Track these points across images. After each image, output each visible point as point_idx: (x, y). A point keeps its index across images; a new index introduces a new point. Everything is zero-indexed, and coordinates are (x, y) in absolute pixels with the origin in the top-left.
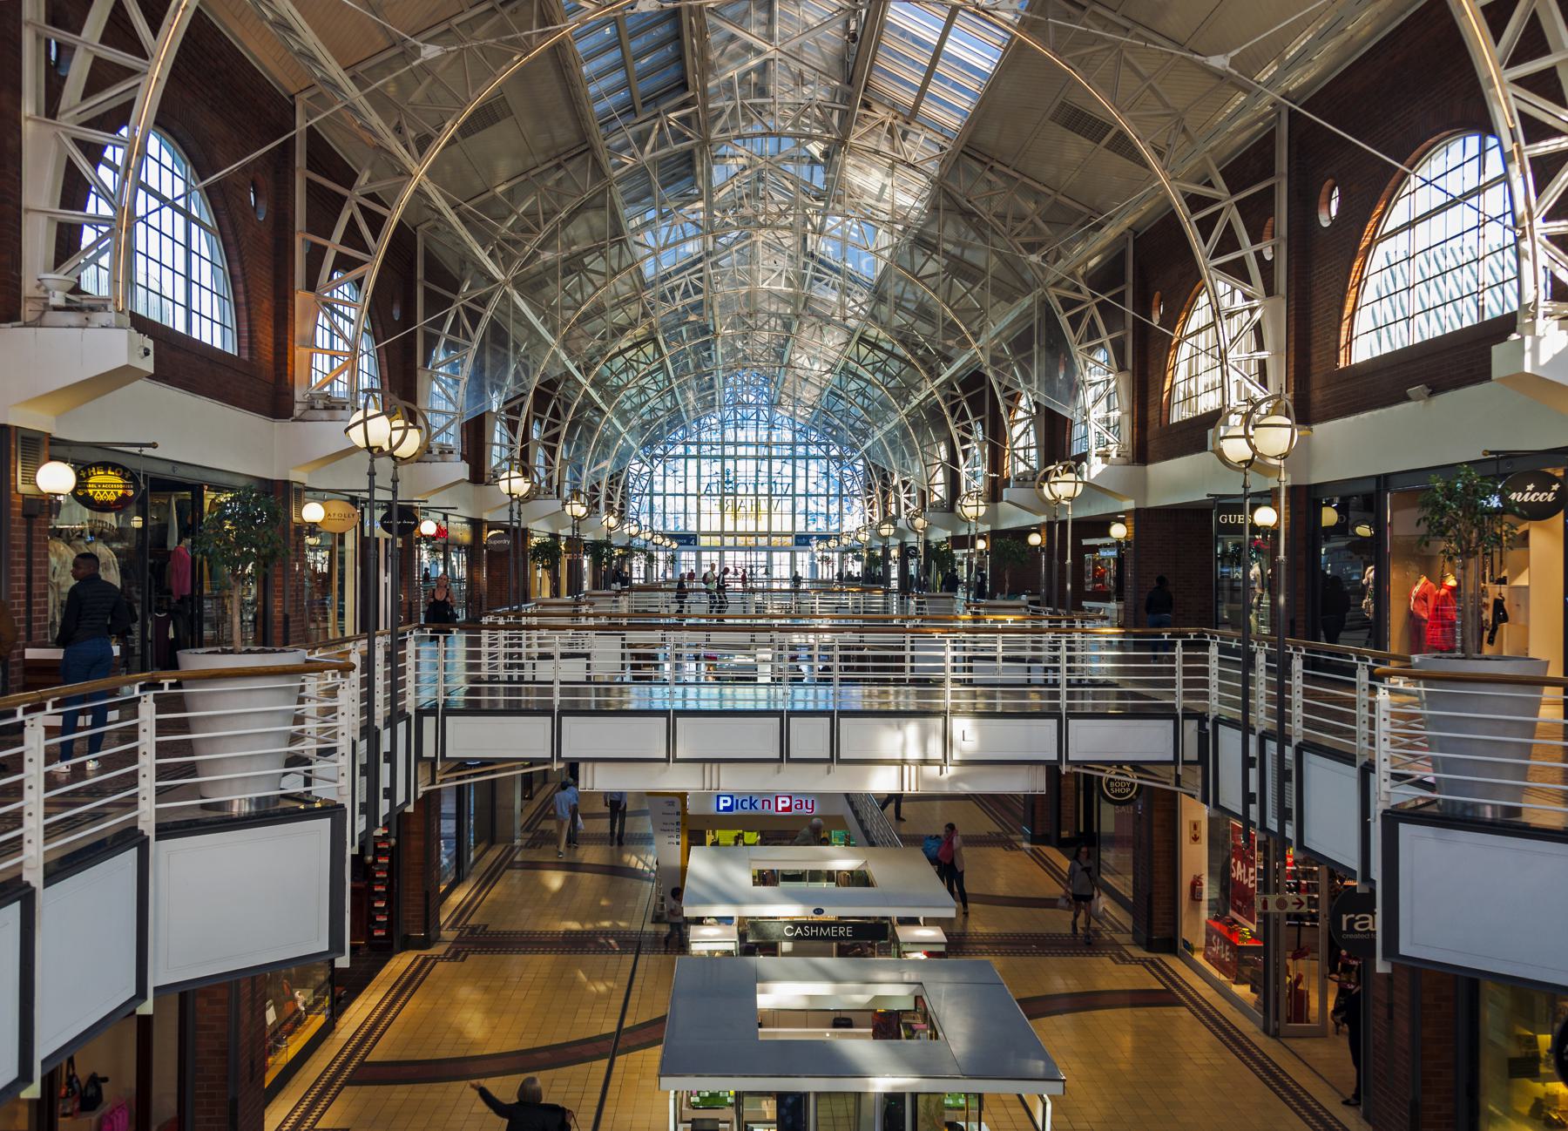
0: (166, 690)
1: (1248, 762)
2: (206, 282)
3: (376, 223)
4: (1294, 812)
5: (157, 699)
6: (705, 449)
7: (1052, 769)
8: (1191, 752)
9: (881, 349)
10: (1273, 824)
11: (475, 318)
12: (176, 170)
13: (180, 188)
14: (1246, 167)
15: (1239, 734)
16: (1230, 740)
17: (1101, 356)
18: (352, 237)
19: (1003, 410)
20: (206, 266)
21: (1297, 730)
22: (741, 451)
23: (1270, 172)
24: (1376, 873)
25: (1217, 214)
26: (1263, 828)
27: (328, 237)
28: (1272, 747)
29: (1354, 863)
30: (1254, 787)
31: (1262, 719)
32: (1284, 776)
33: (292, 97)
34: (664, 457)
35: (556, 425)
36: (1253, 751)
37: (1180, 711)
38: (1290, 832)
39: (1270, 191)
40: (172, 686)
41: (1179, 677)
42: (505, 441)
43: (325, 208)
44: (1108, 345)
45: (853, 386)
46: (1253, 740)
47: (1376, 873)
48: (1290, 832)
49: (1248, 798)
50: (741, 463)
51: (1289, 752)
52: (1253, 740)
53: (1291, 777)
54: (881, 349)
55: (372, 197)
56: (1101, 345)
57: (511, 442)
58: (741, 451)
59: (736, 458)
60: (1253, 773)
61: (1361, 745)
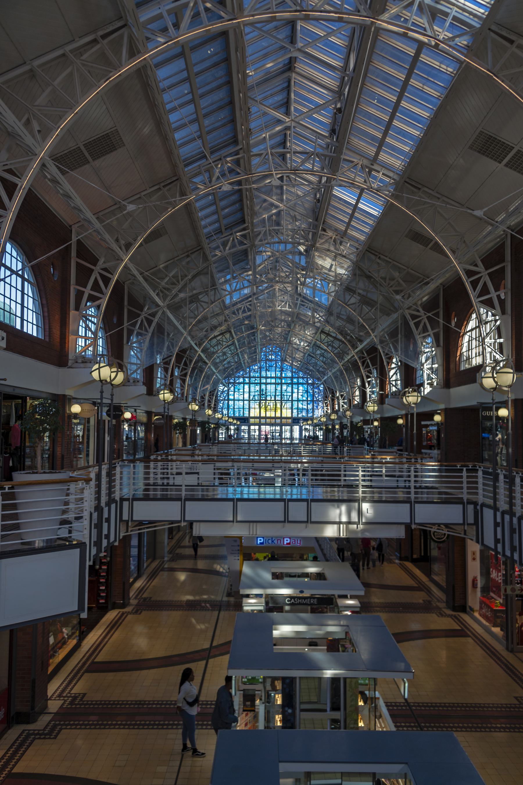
0: (7, 490)
1: (496, 525)
2: (31, 307)
3: (107, 281)
7: (408, 527)
8: (471, 519)
10: (508, 553)
11: (150, 322)
12: (19, 258)
13: (20, 266)
17: (429, 340)
18: (96, 287)
19: (385, 363)
20: (31, 300)
22: (269, 381)
26: (504, 555)
27: (85, 287)
28: (507, 517)
30: (499, 536)
33: (71, 226)
35: (185, 369)
36: (499, 520)
37: (465, 501)
41: (465, 485)
42: (163, 377)
43: (84, 275)
44: (432, 335)
46: (499, 514)
49: (497, 541)
50: (269, 386)
51: (515, 520)
55: (173, 339)
56: (429, 335)
57: (165, 377)
58: (269, 381)
59: (266, 384)
60: (499, 529)
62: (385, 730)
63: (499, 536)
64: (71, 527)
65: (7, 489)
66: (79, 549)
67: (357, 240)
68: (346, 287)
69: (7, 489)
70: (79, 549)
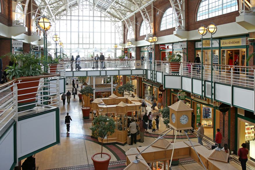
0: (20, 83)
1: (151, 73)
4: (156, 78)
5: (18, 85)
6: (73, 18)
8: (145, 73)
9: (119, 4)
10: (154, 80)
14: (149, 8)
15: (201, 81)
16: (149, 72)
21: (156, 69)
22: (87, 18)
23: (151, 9)
24: (163, 83)
25: (146, 13)
26: (153, 80)
28: (153, 72)
29: (161, 82)
30: (152, 76)
31: (153, 69)
32: (155, 74)
34: (60, 19)
36: (203, 84)
38: (155, 80)
39: (151, 11)
40: (21, 82)
45: (117, 6)
46: (203, 82)
47: (163, 83)
48: (155, 80)
49: (151, 77)
51: (155, 72)
52: (203, 82)
53: (156, 74)
54: (119, 4)
58: (85, 18)
60: (152, 74)
61: (162, 70)
62: (110, 164)
63: (152, 76)
64: (41, 96)
65: (19, 82)
66: (55, 111)
67: (153, 45)
68: (29, 35)
69: (19, 82)
70: (55, 111)
